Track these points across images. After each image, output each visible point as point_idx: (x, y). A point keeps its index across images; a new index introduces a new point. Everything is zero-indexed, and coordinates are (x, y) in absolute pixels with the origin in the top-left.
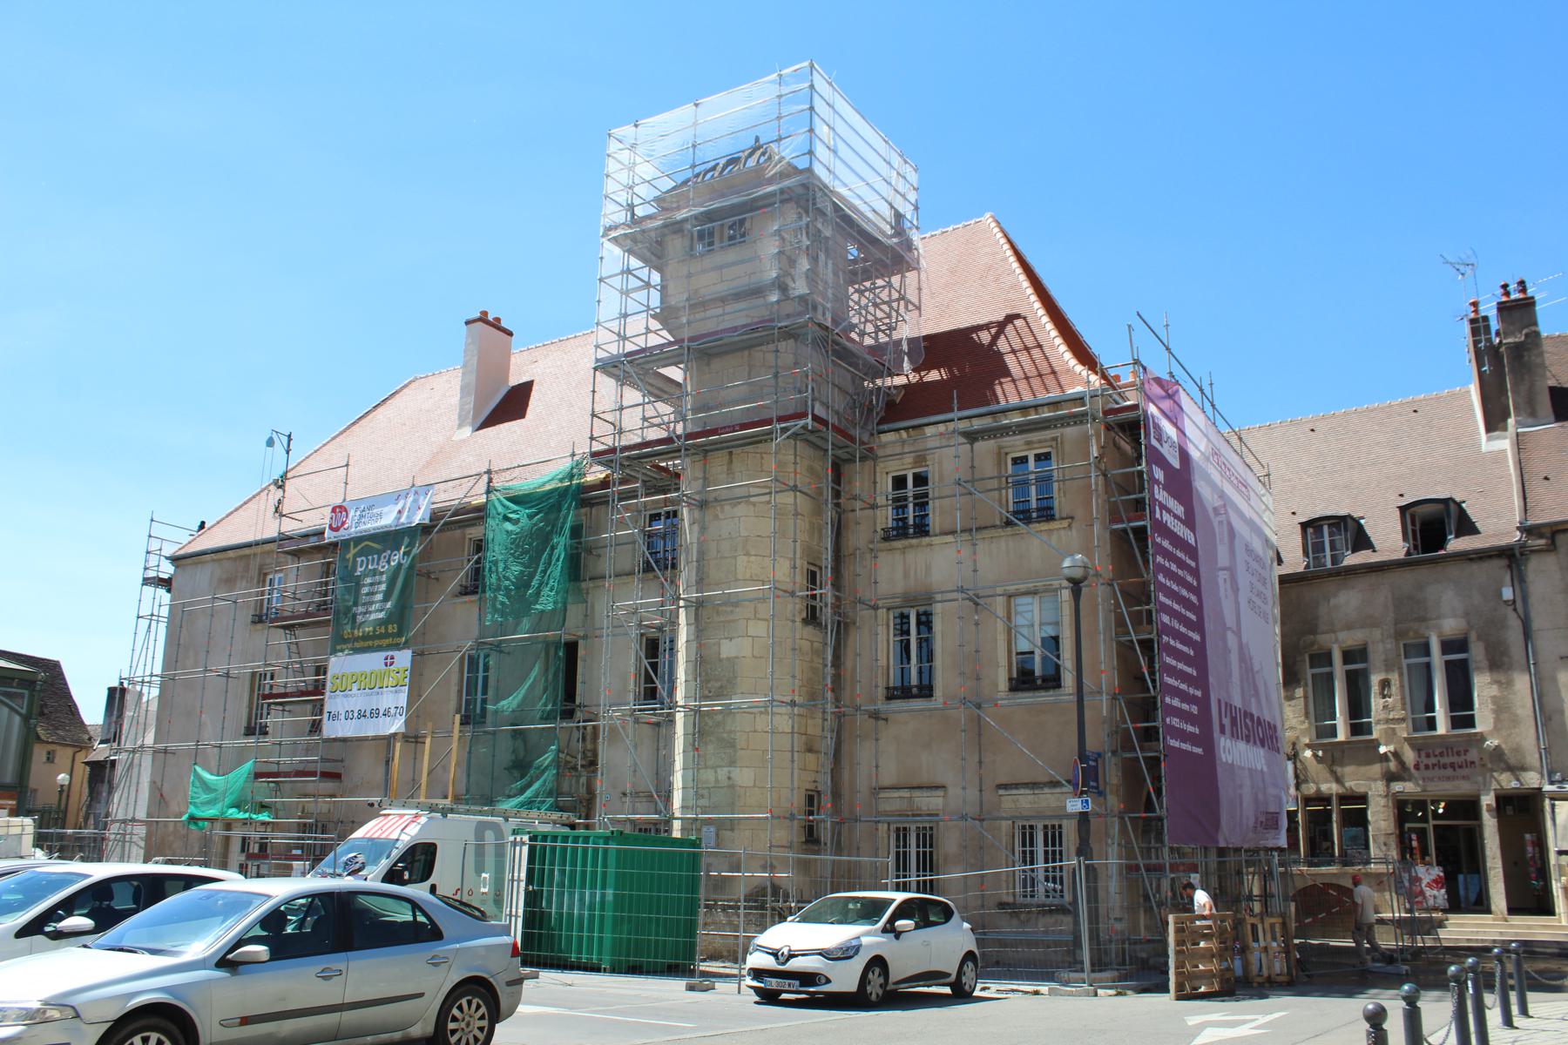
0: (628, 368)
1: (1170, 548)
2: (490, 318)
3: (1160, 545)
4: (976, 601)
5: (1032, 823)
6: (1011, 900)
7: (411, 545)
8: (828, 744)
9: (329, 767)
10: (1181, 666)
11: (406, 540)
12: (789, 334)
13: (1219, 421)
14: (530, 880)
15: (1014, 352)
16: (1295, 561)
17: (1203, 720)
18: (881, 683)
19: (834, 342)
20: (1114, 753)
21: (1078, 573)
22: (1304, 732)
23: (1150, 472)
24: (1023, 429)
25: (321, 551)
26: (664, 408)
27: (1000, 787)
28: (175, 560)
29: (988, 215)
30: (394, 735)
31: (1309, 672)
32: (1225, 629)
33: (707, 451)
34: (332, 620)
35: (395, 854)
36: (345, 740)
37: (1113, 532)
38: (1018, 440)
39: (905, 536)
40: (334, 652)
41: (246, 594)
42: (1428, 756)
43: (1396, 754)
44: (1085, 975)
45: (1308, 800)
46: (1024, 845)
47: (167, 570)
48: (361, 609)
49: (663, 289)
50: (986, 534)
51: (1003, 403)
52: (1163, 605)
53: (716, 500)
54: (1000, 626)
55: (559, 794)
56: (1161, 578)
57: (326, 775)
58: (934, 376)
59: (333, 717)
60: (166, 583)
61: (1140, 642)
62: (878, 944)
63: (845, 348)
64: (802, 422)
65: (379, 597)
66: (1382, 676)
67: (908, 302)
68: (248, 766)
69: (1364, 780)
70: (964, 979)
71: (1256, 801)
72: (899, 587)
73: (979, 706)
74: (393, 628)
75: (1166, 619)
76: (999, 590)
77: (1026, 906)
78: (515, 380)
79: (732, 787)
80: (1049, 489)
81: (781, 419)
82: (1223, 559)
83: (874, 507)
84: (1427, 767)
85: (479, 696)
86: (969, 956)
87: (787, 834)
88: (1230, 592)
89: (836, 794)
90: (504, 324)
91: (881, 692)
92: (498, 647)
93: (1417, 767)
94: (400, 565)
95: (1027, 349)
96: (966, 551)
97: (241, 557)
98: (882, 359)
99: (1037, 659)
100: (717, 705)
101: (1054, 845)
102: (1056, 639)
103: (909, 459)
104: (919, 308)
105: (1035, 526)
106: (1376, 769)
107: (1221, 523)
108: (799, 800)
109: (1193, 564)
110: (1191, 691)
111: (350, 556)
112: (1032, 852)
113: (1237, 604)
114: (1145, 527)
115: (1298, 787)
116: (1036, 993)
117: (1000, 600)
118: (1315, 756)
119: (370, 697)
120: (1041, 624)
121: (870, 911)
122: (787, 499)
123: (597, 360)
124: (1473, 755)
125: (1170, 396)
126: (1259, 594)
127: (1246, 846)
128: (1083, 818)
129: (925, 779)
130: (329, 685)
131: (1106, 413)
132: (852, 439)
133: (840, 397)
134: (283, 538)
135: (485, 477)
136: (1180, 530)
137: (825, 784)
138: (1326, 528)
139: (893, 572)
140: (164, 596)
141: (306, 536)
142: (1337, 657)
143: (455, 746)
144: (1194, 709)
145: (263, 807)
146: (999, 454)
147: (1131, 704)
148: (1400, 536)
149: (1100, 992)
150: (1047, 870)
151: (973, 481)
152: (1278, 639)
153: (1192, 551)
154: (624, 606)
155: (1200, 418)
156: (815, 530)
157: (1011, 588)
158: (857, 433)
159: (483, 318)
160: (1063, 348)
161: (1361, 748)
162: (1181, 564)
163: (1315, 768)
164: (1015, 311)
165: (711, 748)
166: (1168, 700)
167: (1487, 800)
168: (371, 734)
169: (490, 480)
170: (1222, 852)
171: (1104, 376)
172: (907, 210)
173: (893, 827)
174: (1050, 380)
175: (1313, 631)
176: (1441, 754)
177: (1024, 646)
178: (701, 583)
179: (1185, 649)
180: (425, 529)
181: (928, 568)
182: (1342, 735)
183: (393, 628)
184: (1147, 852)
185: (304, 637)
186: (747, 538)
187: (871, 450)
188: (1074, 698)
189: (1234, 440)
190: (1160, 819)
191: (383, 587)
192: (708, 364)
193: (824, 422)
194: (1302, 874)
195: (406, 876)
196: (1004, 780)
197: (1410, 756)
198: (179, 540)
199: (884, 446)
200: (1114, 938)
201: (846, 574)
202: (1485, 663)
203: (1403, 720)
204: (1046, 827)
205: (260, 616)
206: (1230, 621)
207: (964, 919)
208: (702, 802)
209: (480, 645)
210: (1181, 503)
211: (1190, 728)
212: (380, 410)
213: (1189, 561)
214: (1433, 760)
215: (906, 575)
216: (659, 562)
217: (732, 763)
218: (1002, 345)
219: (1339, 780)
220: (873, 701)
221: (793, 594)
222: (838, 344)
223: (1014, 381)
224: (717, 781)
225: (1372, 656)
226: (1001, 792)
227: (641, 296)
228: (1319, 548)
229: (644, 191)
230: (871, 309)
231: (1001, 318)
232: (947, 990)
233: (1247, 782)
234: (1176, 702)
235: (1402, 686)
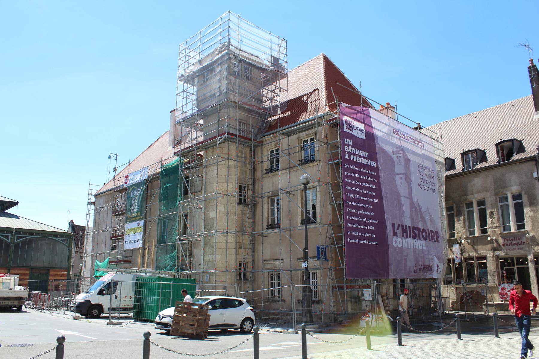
22: (464, 233)
28: (95, 196)
32: (399, 196)
40: (126, 222)
42: (508, 241)
43: (496, 240)
45: (466, 259)
47: (93, 199)
50: (294, 169)
53: (209, 165)
58: (287, 114)
66: (490, 211)
68: (107, 260)
69: (485, 251)
81: (219, 136)
84: (507, 245)
87: (232, 277)
91: (265, 227)
93: (504, 245)
97: (110, 194)
106: (489, 246)
124: (524, 240)
139: (268, 184)
140: (92, 207)
142: (475, 204)
146: (298, 140)
148: (496, 155)
161: (482, 240)
167: (530, 257)
169: (162, 164)
175: (466, 195)
176: (512, 240)
183: (139, 214)
197: (501, 241)
198: (97, 189)
202: (528, 203)
203: (498, 227)
208: (206, 267)
214: (510, 242)
215: (273, 186)
219: (476, 251)
225: (487, 203)
226: (299, 261)
227: (191, 97)
235: (498, 214)
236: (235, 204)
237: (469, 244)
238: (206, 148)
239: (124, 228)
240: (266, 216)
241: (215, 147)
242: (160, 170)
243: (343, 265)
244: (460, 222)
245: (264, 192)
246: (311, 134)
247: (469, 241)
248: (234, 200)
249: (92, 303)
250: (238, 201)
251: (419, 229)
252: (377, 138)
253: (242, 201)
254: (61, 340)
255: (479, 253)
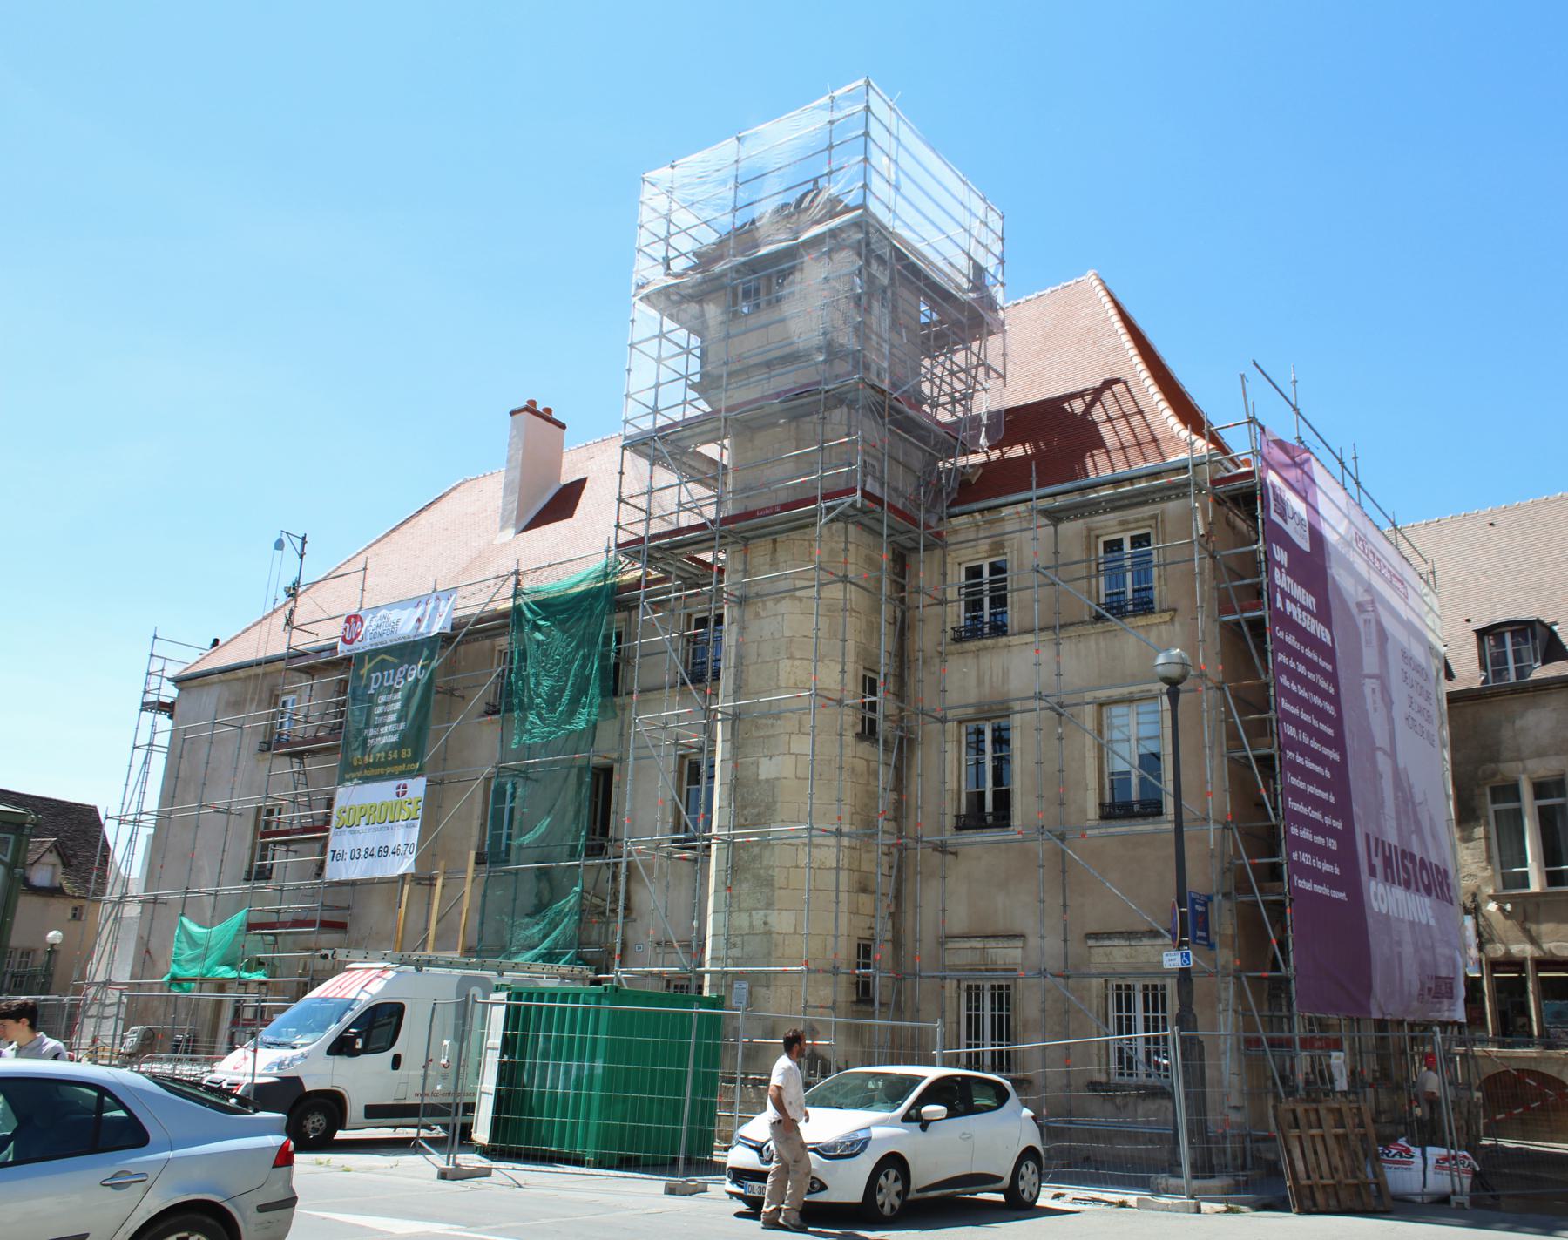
0: (659, 445)
1: (1297, 645)
2: (539, 408)
3: (1283, 641)
4: (1059, 710)
5: (1158, 982)
6: (1103, 1078)
7: (431, 657)
8: (885, 885)
9: (328, 916)
10: (1311, 789)
11: (426, 652)
12: (838, 399)
13: (1365, 501)
14: (504, 1051)
15: (1110, 420)
16: (1469, 674)
17: (1346, 856)
18: (950, 810)
19: (891, 407)
20: (1226, 895)
21: (1175, 671)
22: (1488, 881)
23: (1269, 555)
24: (1115, 505)
25: (341, 670)
26: (699, 491)
27: (1089, 936)
28: (179, 681)
29: (1090, 273)
30: (403, 877)
31: (1491, 809)
32: (1374, 749)
33: (748, 539)
34: (341, 749)
35: (349, 1017)
36: (353, 883)
37: (1224, 625)
38: (1111, 519)
39: (982, 636)
40: (342, 781)
41: (255, 718)
44: (1183, 1182)
45: (1495, 965)
46: (1119, 1010)
47: (170, 693)
48: (372, 732)
49: (703, 358)
50: (1072, 631)
51: (1092, 476)
52: (1286, 713)
53: (758, 595)
54: (1089, 741)
55: (580, 945)
56: (1284, 680)
57: (327, 925)
58: (1017, 451)
59: (337, 856)
60: (168, 708)
61: (1258, 759)
62: (891, 1138)
63: (907, 417)
64: (849, 500)
65: (393, 717)
67: (989, 368)
68: (240, 916)
70: (1022, 1185)
71: (1422, 964)
72: (973, 697)
73: (1062, 838)
74: (407, 753)
75: (1291, 731)
76: (1088, 697)
77: (1121, 1087)
78: (567, 478)
79: (768, 933)
80: (1148, 578)
81: (825, 497)
82: (1370, 661)
83: (943, 602)
85: (505, 832)
86: (1029, 1153)
87: (836, 991)
88: (1380, 704)
89: (897, 943)
90: (555, 416)
91: (950, 821)
92: (523, 774)
94: (417, 680)
95: (1125, 416)
96: (1047, 654)
98: (956, 439)
99: (1134, 780)
100: (752, 835)
101: (1155, 1010)
102: (1157, 756)
103: (984, 546)
104: (1004, 377)
105: (1130, 621)
107: (1367, 621)
108: (846, 951)
109: (1329, 668)
110: (1328, 821)
111: (364, 672)
112: (1129, 1019)
113: (1391, 721)
114: (1262, 619)
115: (1481, 947)
116: (1123, 1204)
117: (1090, 710)
118: (1502, 910)
119: (378, 833)
120: (1138, 740)
121: (896, 1090)
122: (835, 592)
123: (626, 438)
125: (1299, 465)
126: (1420, 711)
127: (1410, 1018)
128: (1184, 975)
129: (1000, 926)
130: (334, 820)
131: (1214, 483)
132: (915, 523)
133: (902, 471)
134: (294, 655)
135: (513, 580)
136: (1312, 625)
137: (883, 930)
138: (1508, 637)
139: (965, 678)
140: (164, 722)
141: (319, 651)
143: (468, 888)
144: (1333, 844)
145: (260, 963)
146: (1088, 536)
147: (1247, 835)
149: (1205, 1206)
150: (1147, 1040)
151: (1056, 567)
152: (1449, 766)
153: (1328, 653)
154: (660, 722)
155: (1339, 496)
156: (872, 629)
157: (1103, 697)
158: (922, 516)
159: (530, 408)
160: (1168, 412)
162: (1312, 666)
163: (1501, 925)
164: (1115, 376)
165: (745, 887)
166: (1294, 830)
168: (377, 875)
169: (518, 583)
170: (1381, 1025)
171: (1214, 439)
172: (990, 264)
173: (964, 985)
174: (1150, 450)
175: (1495, 758)
177: (1120, 766)
178: (738, 691)
179: (1318, 769)
180: (444, 640)
181: (1005, 673)
182: (1535, 885)
183: (407, 753)
184: (1270, 1023)
185: (311, 765)
186: (791, 639)
187: (939, 535)
188: (1172, 826)
189: (1387, 527)
190: (1288, 981)
191: (398, 706)
192: (751, 440)
193: (878, 501)
194: (1489, 1056)
195: (359, 1044)
196: (1095, 928)
198: (186, 659)
199: (955, 532)
200: (1229, 1132)
201: (910, 682)
204: (1146, 987)
205: (269, 744)
206: (1381, 739)
207: (1025, 1104)
208: (735, 952)
209: (500, 771)
210: (1311, 592)
211: (1327, 867)
212: (423, 515)
213: (1323, 664)
215: (980, 682)
216: (700, 672)
217: (769, 905)
218: (1098, 414)
219: (1534, 941)
220: (941, 830)
221: (840, 702)
222: (898, 411)
223: (1108, 452)
224: (751, 926)
226: (1091, 943)
228: (1500, 660)
229: (685, 244)
230: (948, 379)
231: (1098, 385)
232: (1000, 1197)
233: (1408, 937)
234: (1305, 834)
237: (1507, 915)
238: (748, 539)
239: (330, 804)
241: (780, 538)
242: (509, 604)
243: (1286, 962)
244: (1471, 845)
245: (949, 703)
246: (1137, 520)
247: (1508, 907)
249: (309, 1086)
251: (1413, 857)
252: (1331, 550)
255: (1545, 946)
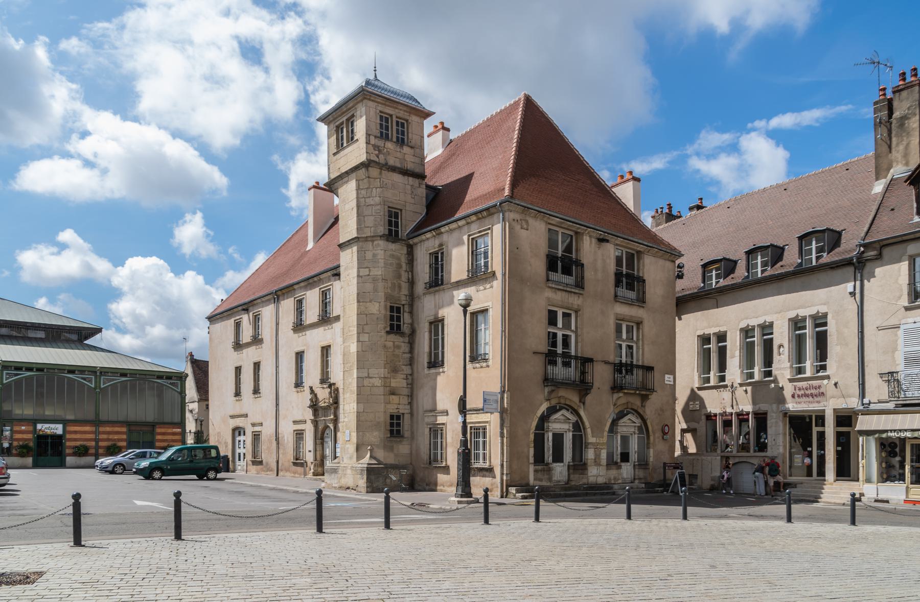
148: (797, 252)
236: (383, 333)
240: (427, 349)
248: (383, 326)
250: (388, 329)
253: (395, 328)
254: (77, 497)
